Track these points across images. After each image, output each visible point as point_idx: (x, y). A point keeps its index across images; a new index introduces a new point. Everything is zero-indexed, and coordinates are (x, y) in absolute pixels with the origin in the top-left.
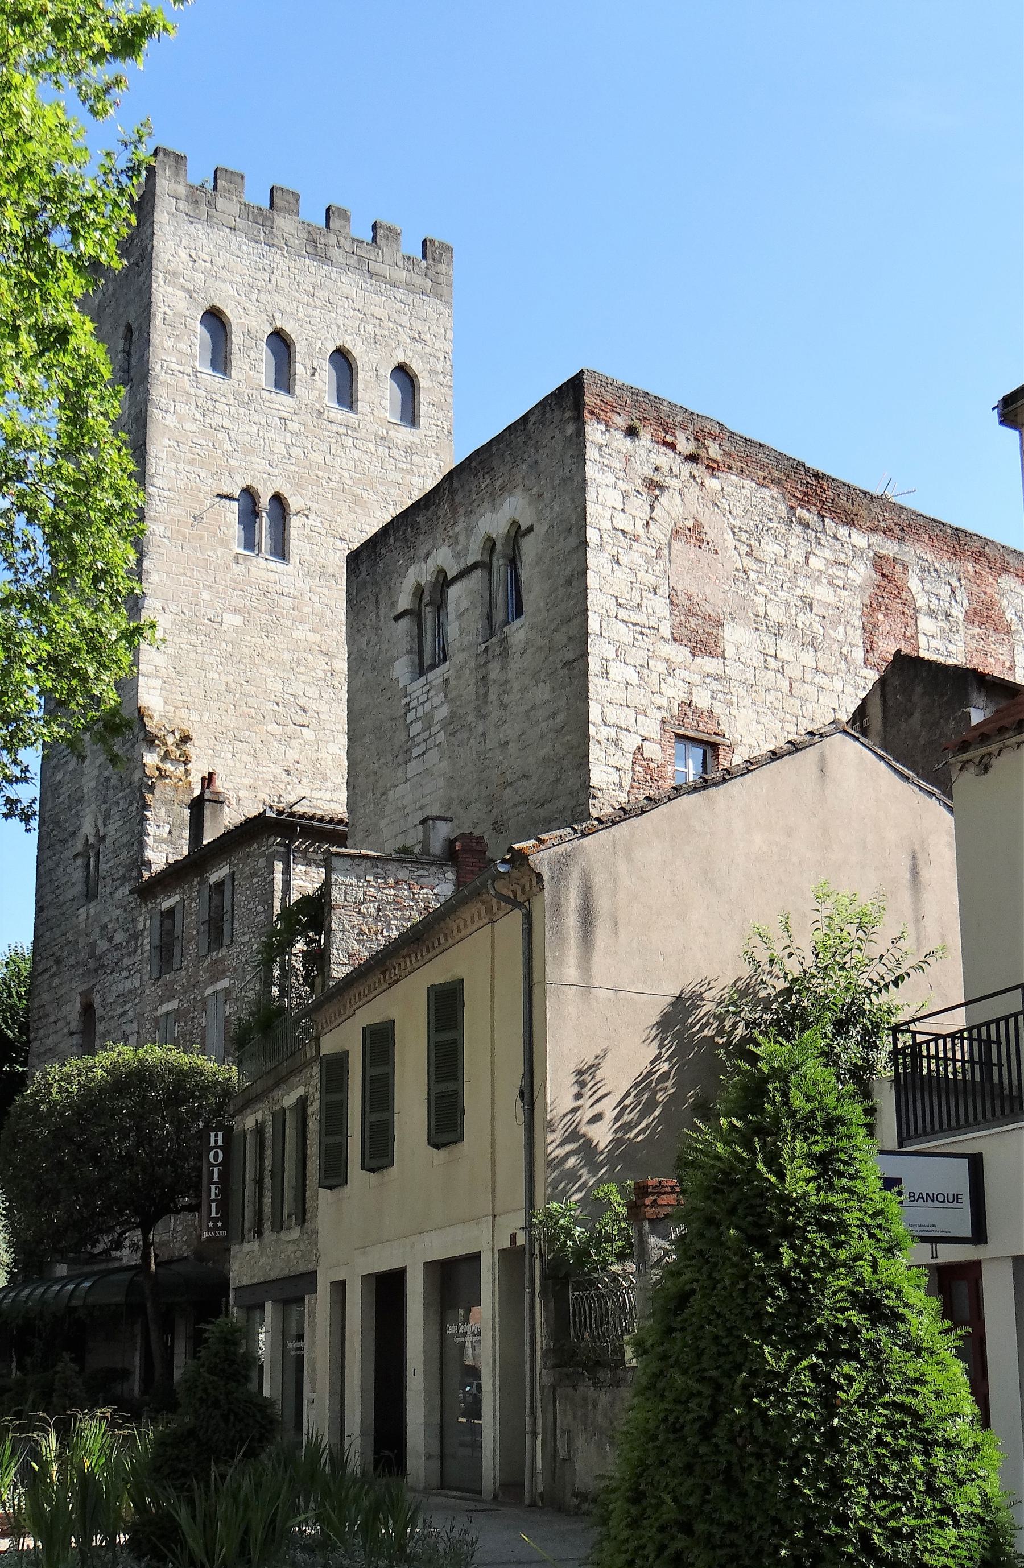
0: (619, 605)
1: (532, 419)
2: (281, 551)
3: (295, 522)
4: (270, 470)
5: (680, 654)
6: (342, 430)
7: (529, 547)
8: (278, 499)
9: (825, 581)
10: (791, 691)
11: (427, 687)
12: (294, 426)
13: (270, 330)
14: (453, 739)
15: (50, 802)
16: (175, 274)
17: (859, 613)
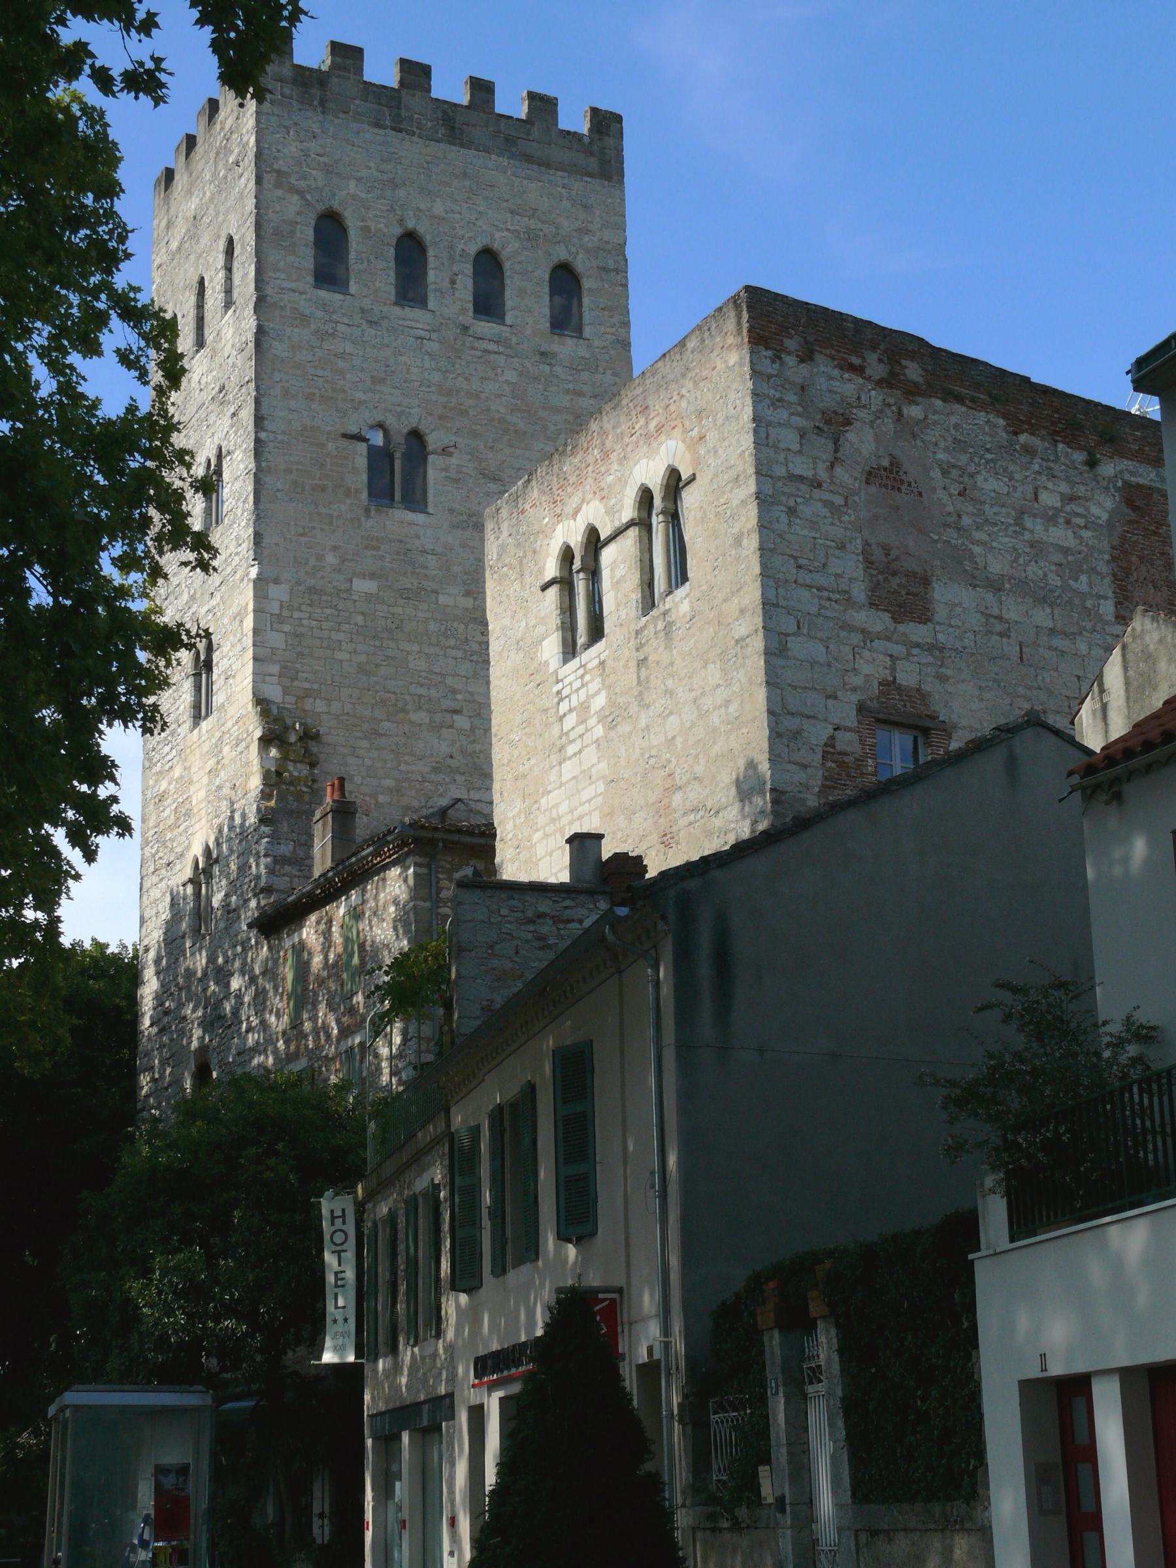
0: (799, 567)
5: (879, 621)
6: (492, 347)
7: (690, 499)
9: (1061, 520)
10: (1021, 658)
11: (581, 671)
12: (433, 346)
13: (398, 231)
14: (613, 733)
15: (154, 817)
17: (1107, 557)
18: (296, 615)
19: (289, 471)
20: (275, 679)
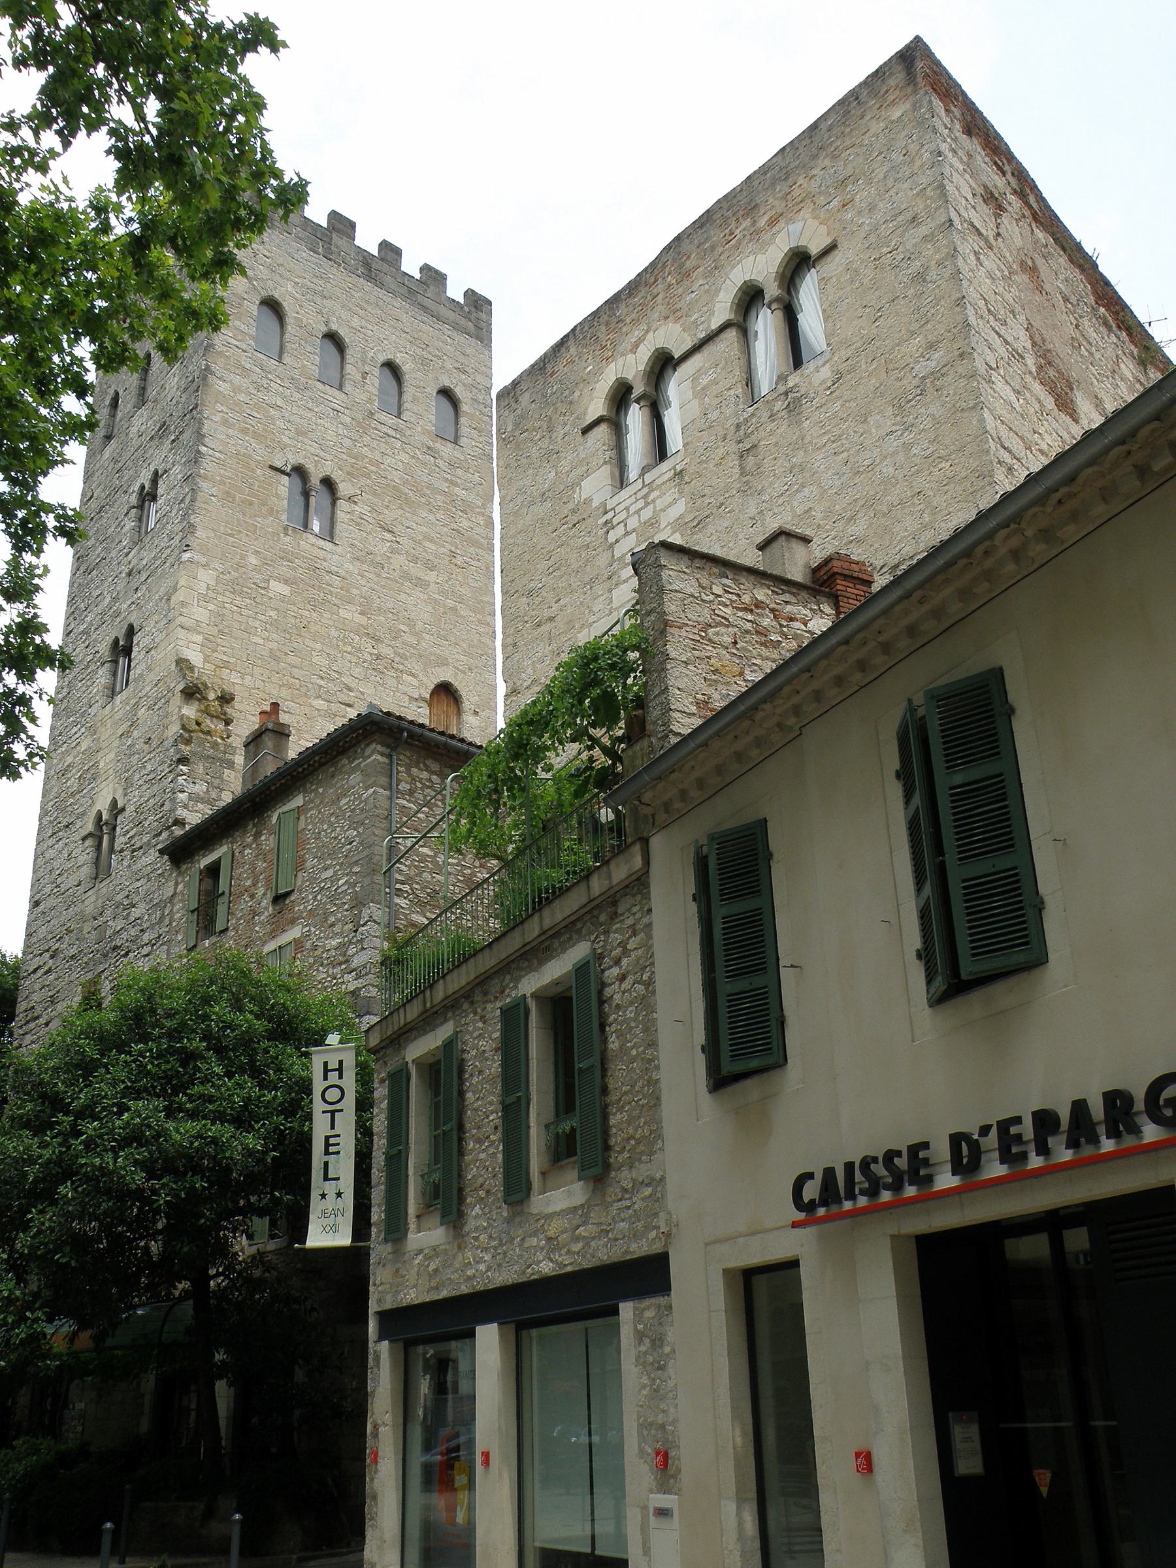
1: (824, 126)
2: (330, 533)
4: (322, 454)
6: (391, 432)
18: (220, 598)
19: (223, 483)
20: (198, 648)
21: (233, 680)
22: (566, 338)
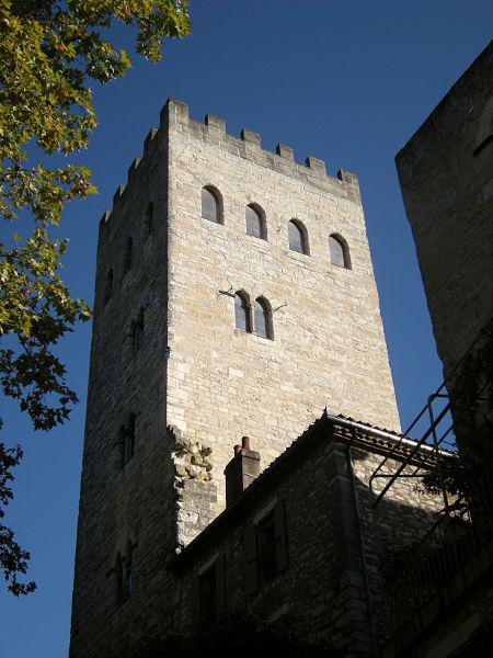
2: (269, 335)
3: (275, 317)
6: (301, 264)
8: (261, 300)
16: (182, 163)
20: (182, 418)
21: (209, 440)
22: (447, 96)
